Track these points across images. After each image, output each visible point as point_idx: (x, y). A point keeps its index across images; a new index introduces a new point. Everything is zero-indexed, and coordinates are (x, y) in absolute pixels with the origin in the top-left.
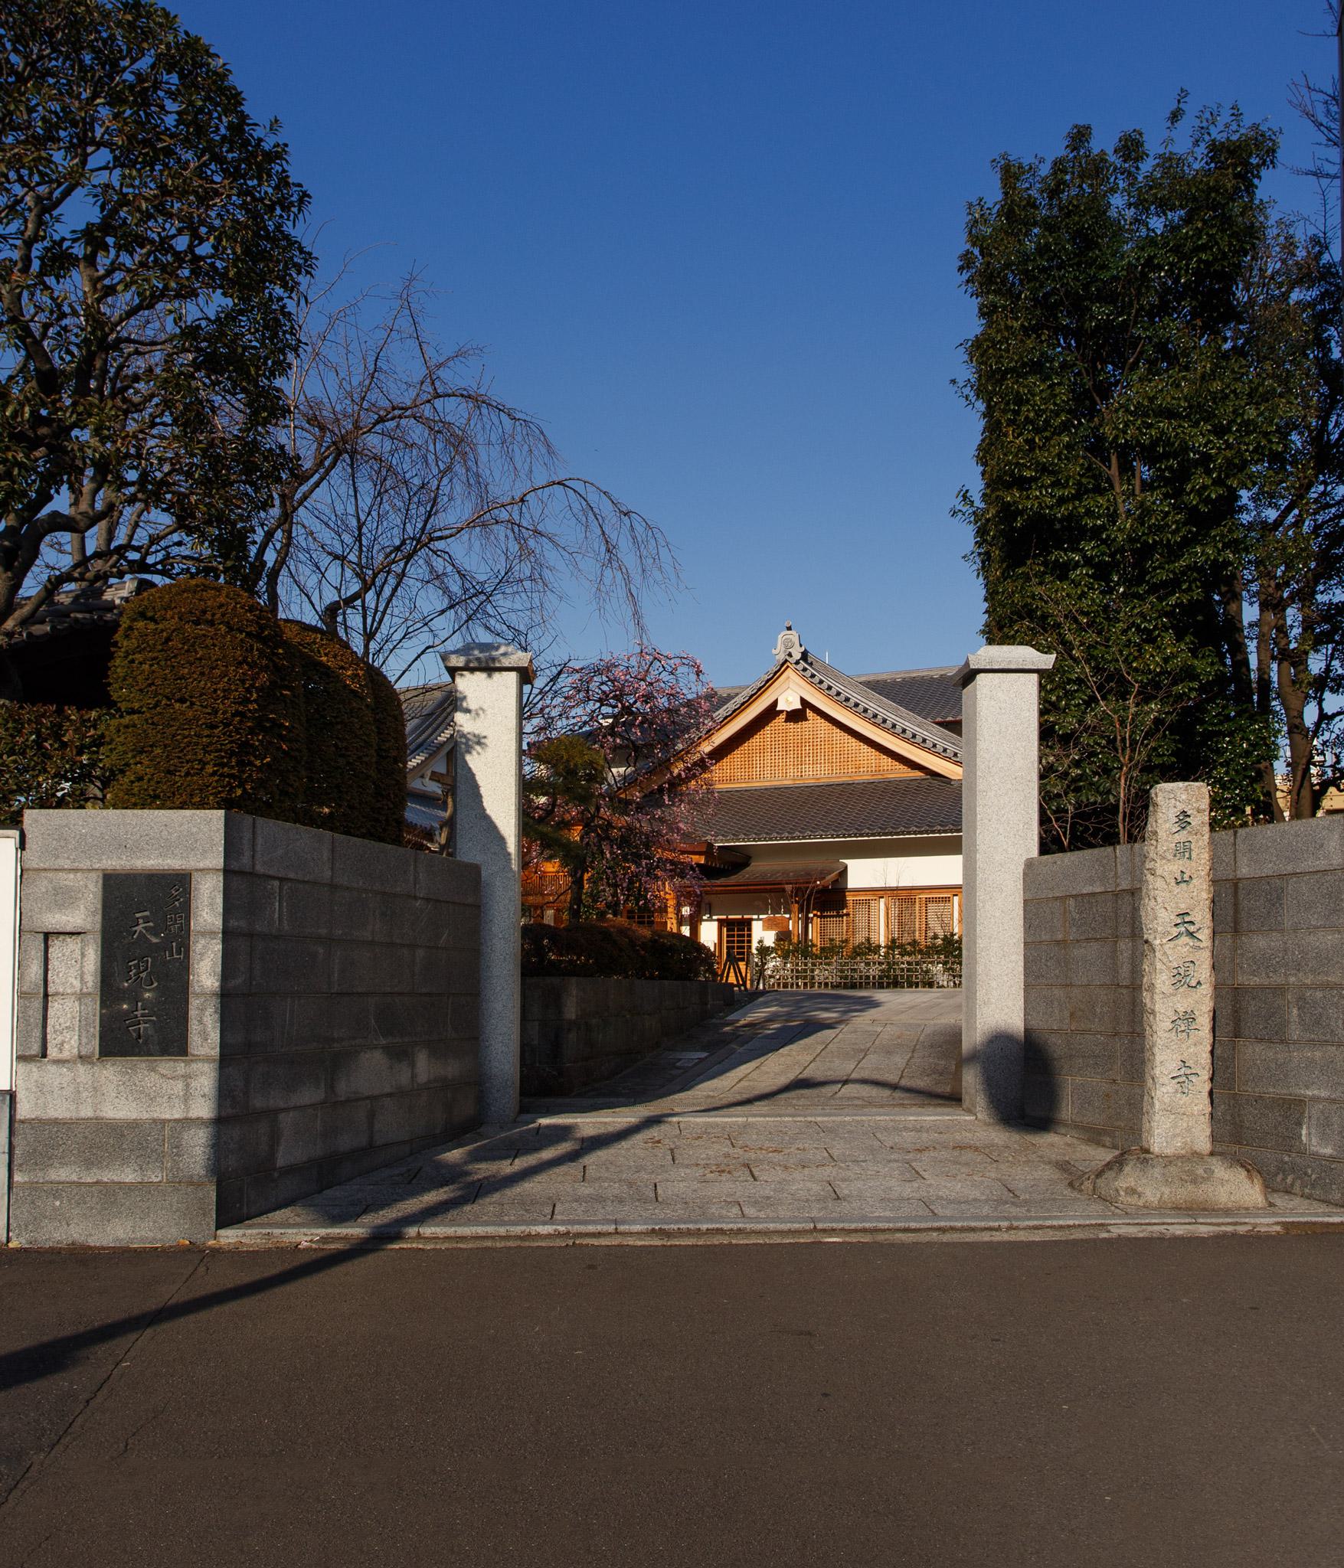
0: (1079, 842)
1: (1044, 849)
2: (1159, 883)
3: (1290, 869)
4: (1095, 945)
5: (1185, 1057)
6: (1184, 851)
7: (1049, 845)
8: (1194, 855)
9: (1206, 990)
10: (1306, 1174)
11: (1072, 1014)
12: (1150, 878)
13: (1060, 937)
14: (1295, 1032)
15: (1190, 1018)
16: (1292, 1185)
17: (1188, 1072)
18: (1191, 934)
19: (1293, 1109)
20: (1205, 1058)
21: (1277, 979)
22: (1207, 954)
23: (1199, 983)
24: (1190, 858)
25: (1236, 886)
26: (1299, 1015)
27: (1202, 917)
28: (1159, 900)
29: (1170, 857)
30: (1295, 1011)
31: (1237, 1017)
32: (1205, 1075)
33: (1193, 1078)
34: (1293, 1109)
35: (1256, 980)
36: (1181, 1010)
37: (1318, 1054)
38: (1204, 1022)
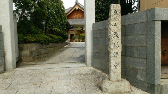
0: (101, 20)
1: (96, 22)
2: (111, 26)
3: (135, 22)
4: (102, 38)
5: (116, 61)
6: (116, 19)
7: (97, 20)
8: (118, 19)
9: (120, 47)
10: (138, 84)
11: (99, 50)
12: (110, 25)
13: (98, 37)
14: (136, 55)
15: (117, 53)
16: (135, 85)
17: (117, 64)
18: (117, 36)
19: (136, 70)
20: (120, 61)
21: (133, 45)
22: (120, 40)
23: (119, 46)
24: (117, 20)
25: (125, 26)
26: (137, 52)
27: (119, 33)
28: (111, 29)
29: (113, 20)
30: (136, 51)
31: (125, 53)
32: (120, 65)
33: (118, 65)
34: (136, 70)
35: (129, 45)
36: (116, 52)
37: (141, 60)
38: (120, 54)
